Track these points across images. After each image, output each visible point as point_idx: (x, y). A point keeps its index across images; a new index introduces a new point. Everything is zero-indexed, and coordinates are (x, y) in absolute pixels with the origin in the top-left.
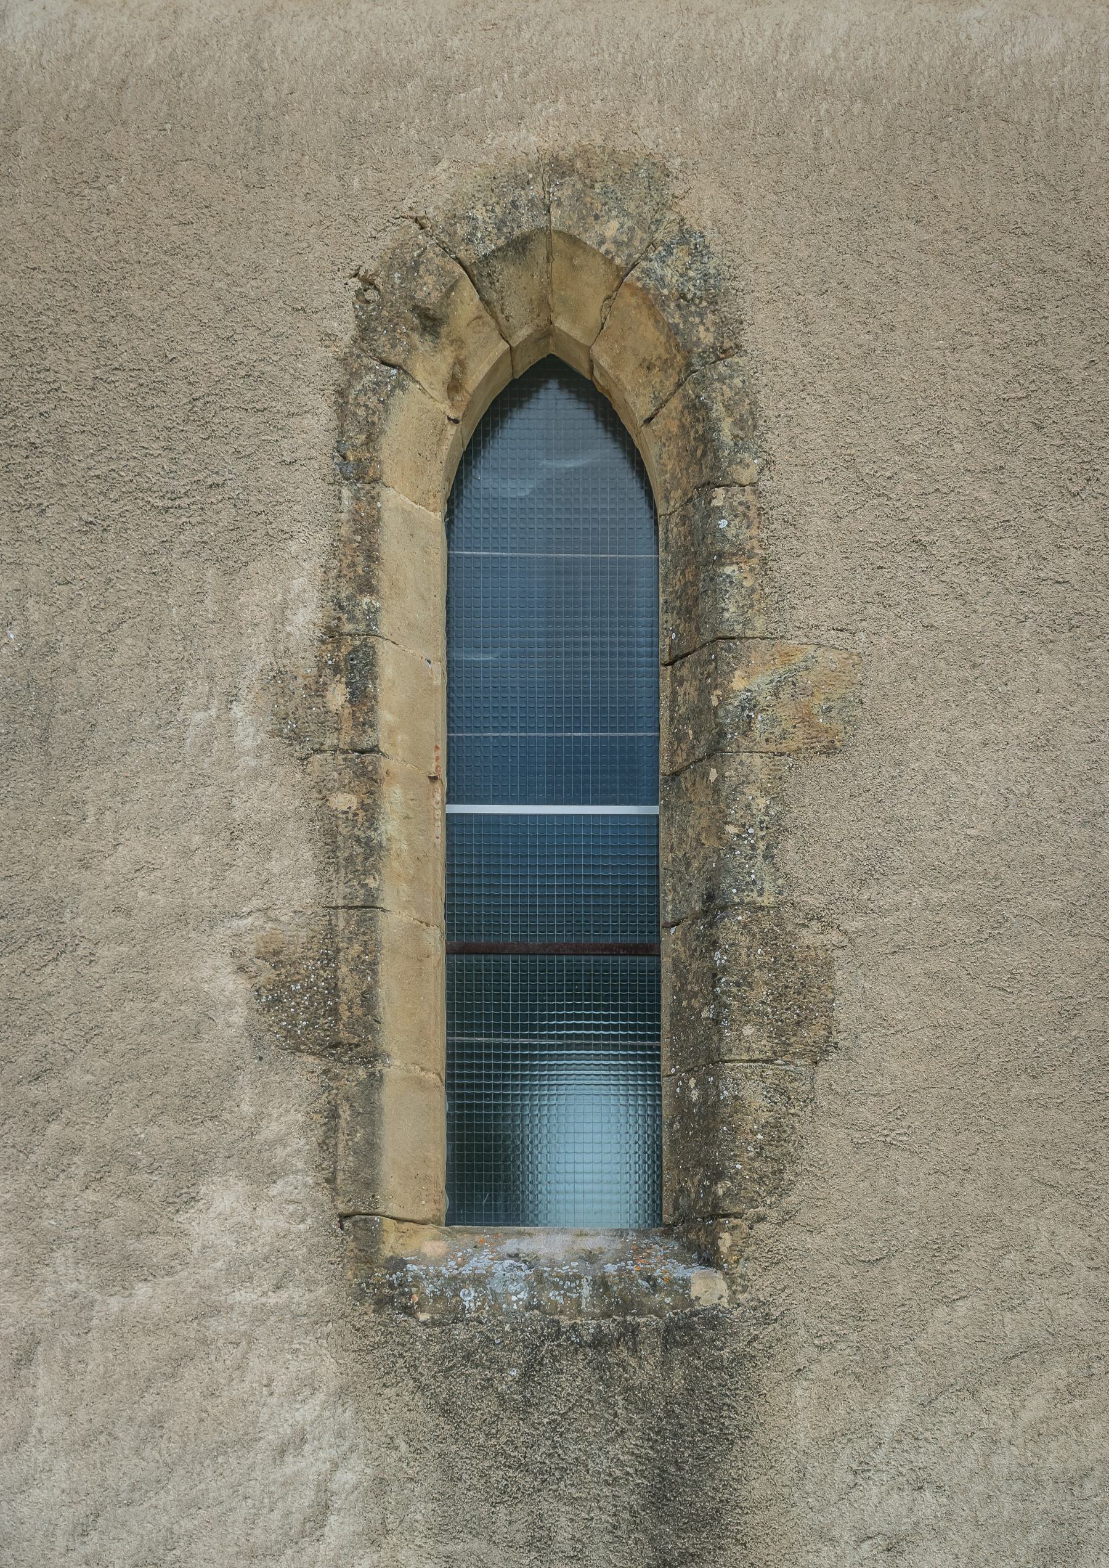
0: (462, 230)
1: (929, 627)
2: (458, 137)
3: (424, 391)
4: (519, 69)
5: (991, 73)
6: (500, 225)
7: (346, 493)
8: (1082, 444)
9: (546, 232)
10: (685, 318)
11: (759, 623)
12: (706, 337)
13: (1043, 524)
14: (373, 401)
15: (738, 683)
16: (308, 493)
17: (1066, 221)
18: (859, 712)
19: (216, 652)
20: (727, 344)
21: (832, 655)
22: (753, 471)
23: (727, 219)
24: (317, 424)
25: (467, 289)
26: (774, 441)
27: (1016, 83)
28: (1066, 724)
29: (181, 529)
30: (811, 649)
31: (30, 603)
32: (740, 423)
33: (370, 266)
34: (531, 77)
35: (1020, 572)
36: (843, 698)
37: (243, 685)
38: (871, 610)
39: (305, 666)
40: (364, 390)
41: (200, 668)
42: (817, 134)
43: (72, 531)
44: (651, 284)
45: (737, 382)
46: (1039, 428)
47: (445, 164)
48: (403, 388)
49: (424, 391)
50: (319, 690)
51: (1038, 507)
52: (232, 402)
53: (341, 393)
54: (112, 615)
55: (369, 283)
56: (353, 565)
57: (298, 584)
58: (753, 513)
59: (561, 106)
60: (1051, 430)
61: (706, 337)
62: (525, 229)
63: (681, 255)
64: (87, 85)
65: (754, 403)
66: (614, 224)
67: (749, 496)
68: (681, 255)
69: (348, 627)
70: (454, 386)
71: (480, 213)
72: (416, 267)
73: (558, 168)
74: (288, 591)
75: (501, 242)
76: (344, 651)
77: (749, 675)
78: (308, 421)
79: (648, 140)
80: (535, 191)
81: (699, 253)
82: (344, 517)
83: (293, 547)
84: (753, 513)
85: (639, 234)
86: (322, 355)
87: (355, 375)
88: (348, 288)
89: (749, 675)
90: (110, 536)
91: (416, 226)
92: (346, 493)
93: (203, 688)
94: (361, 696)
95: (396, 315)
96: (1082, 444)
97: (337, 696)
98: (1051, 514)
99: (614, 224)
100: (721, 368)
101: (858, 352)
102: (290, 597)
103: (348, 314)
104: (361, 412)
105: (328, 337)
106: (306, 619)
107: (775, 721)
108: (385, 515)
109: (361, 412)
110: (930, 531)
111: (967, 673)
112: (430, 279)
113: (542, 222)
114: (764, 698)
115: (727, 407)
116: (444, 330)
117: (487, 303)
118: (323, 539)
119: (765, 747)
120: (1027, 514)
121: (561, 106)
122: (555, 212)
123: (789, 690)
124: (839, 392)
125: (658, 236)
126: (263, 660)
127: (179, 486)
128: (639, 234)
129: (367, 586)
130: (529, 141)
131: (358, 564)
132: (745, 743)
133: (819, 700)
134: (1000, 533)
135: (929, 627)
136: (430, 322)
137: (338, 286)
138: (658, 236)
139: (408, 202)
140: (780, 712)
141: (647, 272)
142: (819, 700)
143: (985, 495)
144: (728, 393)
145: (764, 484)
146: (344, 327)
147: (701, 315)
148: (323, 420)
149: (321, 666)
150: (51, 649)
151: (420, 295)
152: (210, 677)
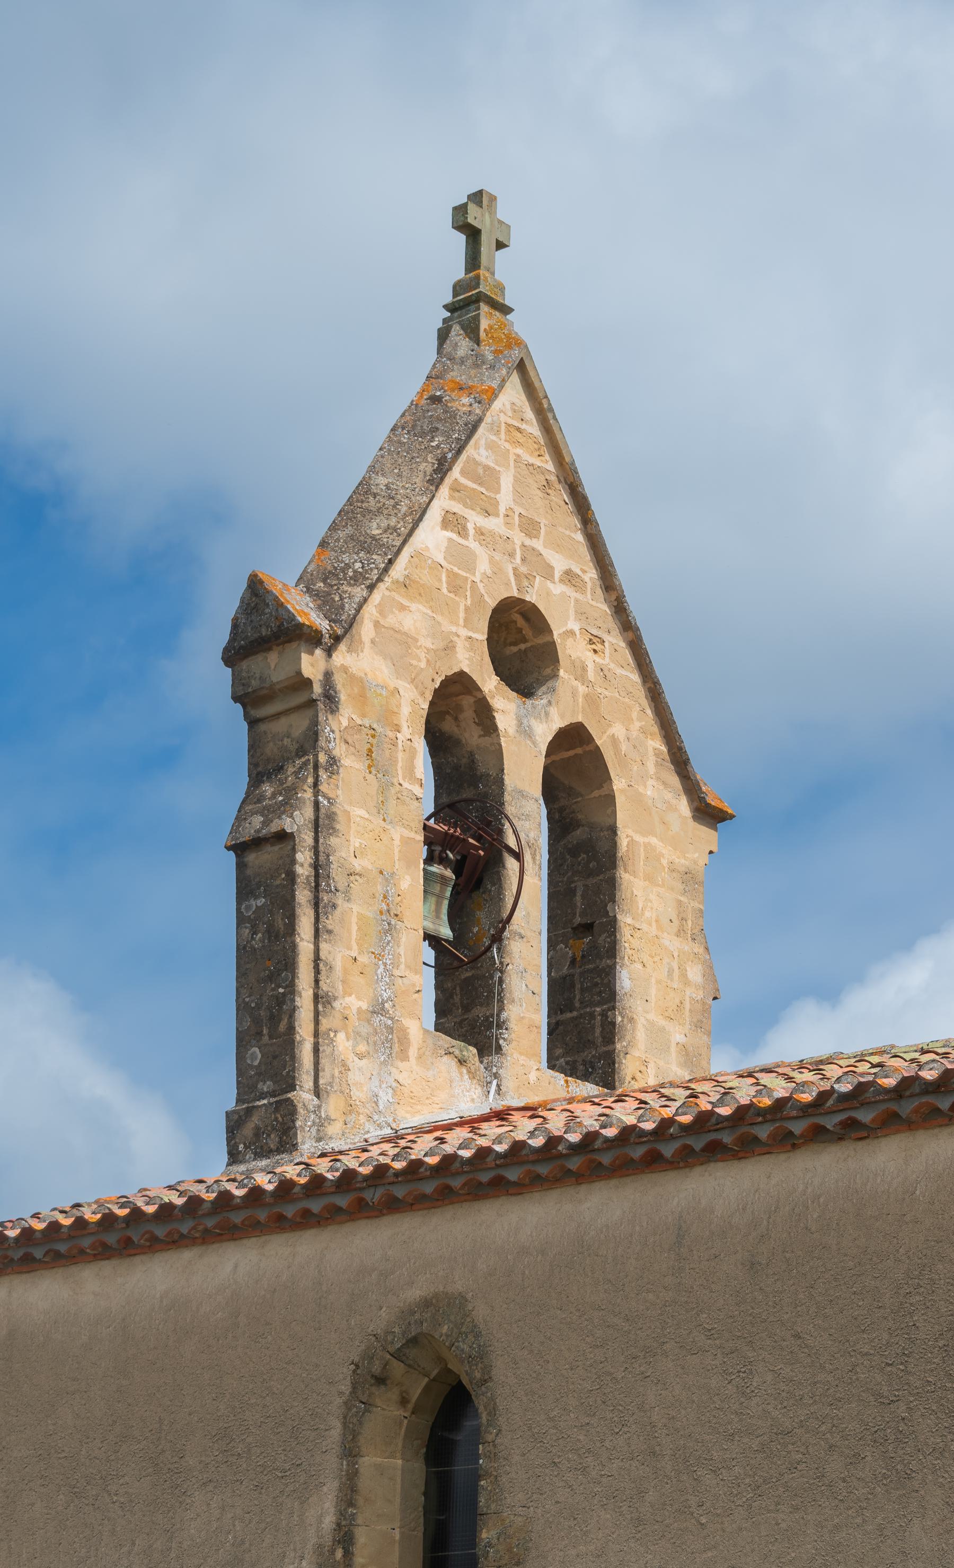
0: (390, 1338)
1: (557, 1502)
2: (390, 1296)
3: (383, 1409)
4: (412, 1261)
5: (592, 1233)
6: (404, 1333)
7: (345, 1463)
8: (621, 1408)
9: (421, 1333)
10: (470, 1367)
11: (493, 1506)
12: (478, 1375)
13: (604, 1449)
14: (355, 1420)
15: (484, 1535)
16: (330, 1464)
17: (618, 1301)
18: (530, 1545)
19: (297, 1539)
20: (486, 1377)
21: (520, 1519)
22: (493, 1435)
23: (488, 1319)
24: (336, 1432)
25: (395, 1363)
26: (502, 1420)
27: (602, 1236)
28: (610, 1544)
29: (287, 1485)
30: (512, 1517)
31: (237, 1523)
32: (489, 1414)
33: (356, 1359)
34: (417, 1264)
35: (594, 1473)
36: (524, 1538)
37: (306, 1552)
38: (535, 1496)
39: (328, 1540)
40: (352, 1416)
41: (292, 1547)
42: (524, 1273)
43: (251, 1490)
44: (458, 1352)
45: (489, 1394)
46: (604, 1402)
47: (384, 1309)
48: (370, 1412)
49: (383, 1409)
50: (332, 1552)
51: (602, 1441)
52: (306, 1426)
53: (345, 1418)
54: (263, 1525)
55: (357, 1366)
56: (346, 1495)
57: (327, 1505)
58: (492, 1456)
59: (428, 1276)
60: (609, 1403)
61: (478, 1375)
62: (413, 1334)
63: (471, 1337)
64: (263, 1293)
65: (495, 1404)
66: (446, 1327)
67: (491, 1448)
68: (471, 1337)
69: (344, 1523)
70: (404, 1402)
71: (396, 1330)
72: (372, 1358)
73: (426, 1303)
74: (322, 1509)
75: (404, 1341)
76: (342, 1533)
77: (488, 1531)
78: (333, 1432)
79: (459, 1286)
80: (417, 1316)
81: (478, 1335)
82: (344, 1473)
83: (325, 1489)
84: (492, 1456)
85: (455, 1330)
86: (339, 1401)
87: (349, 1409)
88: (347, 1370)
89: (488, 1531)
90: (263, 1491)
91: (374, 1339)
92: (345, 1463)
93: (292, 1555)
94: (348, 1554)
95: (371, 1379)
96: (621, 1408)
97: (339, 1554)
98: (607, 1444)
99: (446, 1327)
100: (483, 1388)
101: (534, 1375)
102: (323, 1514)
103: (348, 1382)
104: (351, 1426)
105: (341, 1393)
106: (329, 1521)
107: (498, 1551)
108: (362, 1470)
109: (351, 1426)
110: (559, 1457)
111: (572, 1523)
112: (377, 1362)
113: (419, 1330)
114: (495, 1541)
115: (485, 1407)
116: (388, 1382)
117: (410, 1366)
118: (336, 1484)
119: (494, 1564)
120: (598, 1444)
121: (428, 1276)
122: (425, 1324)
123: (503, 1536)
124: (527, 1395)
125: (463, 1330)
126: (314, 1540)
127: (287, 1466)
128: (455, 1330)
129: (351, 1504)
130: (414, 1294)
131: (349, 1496)
132: (486, 1563)
133: (515, 1541)
134: (586, 1455)
135: (557, 1502)
136: (380, 1381)
137: (345, 1370)
138: (463, 1330)
139: (371, 1328)
140: (500, 1547)
141: (457, 1347)
142: (515, 1541)
143: (582, 1438)
144: (485, 1400)
145: (498, 1441)
146: (346, 1388)
147: (476, 1365)
148: (338, 1430)
149: (334, 1540)
150: (243, 1542)
151: (373, 1370)
152: (295, 1550)
